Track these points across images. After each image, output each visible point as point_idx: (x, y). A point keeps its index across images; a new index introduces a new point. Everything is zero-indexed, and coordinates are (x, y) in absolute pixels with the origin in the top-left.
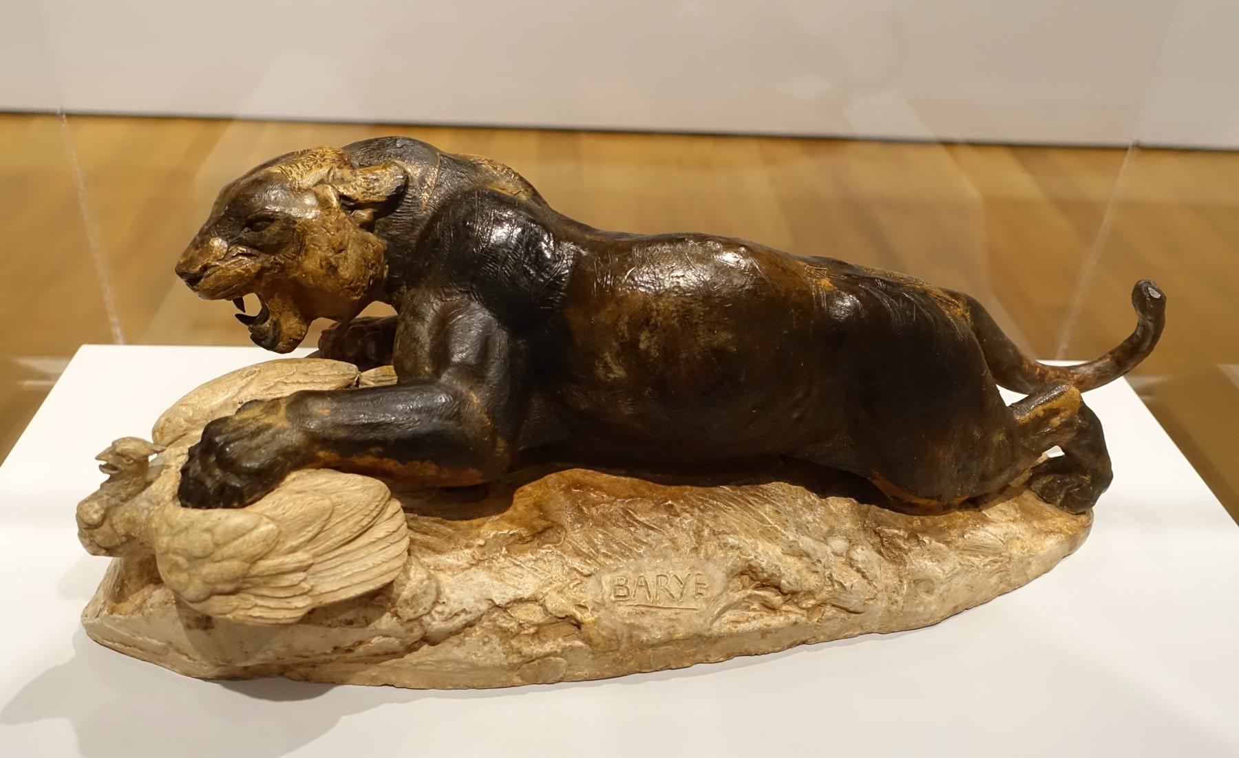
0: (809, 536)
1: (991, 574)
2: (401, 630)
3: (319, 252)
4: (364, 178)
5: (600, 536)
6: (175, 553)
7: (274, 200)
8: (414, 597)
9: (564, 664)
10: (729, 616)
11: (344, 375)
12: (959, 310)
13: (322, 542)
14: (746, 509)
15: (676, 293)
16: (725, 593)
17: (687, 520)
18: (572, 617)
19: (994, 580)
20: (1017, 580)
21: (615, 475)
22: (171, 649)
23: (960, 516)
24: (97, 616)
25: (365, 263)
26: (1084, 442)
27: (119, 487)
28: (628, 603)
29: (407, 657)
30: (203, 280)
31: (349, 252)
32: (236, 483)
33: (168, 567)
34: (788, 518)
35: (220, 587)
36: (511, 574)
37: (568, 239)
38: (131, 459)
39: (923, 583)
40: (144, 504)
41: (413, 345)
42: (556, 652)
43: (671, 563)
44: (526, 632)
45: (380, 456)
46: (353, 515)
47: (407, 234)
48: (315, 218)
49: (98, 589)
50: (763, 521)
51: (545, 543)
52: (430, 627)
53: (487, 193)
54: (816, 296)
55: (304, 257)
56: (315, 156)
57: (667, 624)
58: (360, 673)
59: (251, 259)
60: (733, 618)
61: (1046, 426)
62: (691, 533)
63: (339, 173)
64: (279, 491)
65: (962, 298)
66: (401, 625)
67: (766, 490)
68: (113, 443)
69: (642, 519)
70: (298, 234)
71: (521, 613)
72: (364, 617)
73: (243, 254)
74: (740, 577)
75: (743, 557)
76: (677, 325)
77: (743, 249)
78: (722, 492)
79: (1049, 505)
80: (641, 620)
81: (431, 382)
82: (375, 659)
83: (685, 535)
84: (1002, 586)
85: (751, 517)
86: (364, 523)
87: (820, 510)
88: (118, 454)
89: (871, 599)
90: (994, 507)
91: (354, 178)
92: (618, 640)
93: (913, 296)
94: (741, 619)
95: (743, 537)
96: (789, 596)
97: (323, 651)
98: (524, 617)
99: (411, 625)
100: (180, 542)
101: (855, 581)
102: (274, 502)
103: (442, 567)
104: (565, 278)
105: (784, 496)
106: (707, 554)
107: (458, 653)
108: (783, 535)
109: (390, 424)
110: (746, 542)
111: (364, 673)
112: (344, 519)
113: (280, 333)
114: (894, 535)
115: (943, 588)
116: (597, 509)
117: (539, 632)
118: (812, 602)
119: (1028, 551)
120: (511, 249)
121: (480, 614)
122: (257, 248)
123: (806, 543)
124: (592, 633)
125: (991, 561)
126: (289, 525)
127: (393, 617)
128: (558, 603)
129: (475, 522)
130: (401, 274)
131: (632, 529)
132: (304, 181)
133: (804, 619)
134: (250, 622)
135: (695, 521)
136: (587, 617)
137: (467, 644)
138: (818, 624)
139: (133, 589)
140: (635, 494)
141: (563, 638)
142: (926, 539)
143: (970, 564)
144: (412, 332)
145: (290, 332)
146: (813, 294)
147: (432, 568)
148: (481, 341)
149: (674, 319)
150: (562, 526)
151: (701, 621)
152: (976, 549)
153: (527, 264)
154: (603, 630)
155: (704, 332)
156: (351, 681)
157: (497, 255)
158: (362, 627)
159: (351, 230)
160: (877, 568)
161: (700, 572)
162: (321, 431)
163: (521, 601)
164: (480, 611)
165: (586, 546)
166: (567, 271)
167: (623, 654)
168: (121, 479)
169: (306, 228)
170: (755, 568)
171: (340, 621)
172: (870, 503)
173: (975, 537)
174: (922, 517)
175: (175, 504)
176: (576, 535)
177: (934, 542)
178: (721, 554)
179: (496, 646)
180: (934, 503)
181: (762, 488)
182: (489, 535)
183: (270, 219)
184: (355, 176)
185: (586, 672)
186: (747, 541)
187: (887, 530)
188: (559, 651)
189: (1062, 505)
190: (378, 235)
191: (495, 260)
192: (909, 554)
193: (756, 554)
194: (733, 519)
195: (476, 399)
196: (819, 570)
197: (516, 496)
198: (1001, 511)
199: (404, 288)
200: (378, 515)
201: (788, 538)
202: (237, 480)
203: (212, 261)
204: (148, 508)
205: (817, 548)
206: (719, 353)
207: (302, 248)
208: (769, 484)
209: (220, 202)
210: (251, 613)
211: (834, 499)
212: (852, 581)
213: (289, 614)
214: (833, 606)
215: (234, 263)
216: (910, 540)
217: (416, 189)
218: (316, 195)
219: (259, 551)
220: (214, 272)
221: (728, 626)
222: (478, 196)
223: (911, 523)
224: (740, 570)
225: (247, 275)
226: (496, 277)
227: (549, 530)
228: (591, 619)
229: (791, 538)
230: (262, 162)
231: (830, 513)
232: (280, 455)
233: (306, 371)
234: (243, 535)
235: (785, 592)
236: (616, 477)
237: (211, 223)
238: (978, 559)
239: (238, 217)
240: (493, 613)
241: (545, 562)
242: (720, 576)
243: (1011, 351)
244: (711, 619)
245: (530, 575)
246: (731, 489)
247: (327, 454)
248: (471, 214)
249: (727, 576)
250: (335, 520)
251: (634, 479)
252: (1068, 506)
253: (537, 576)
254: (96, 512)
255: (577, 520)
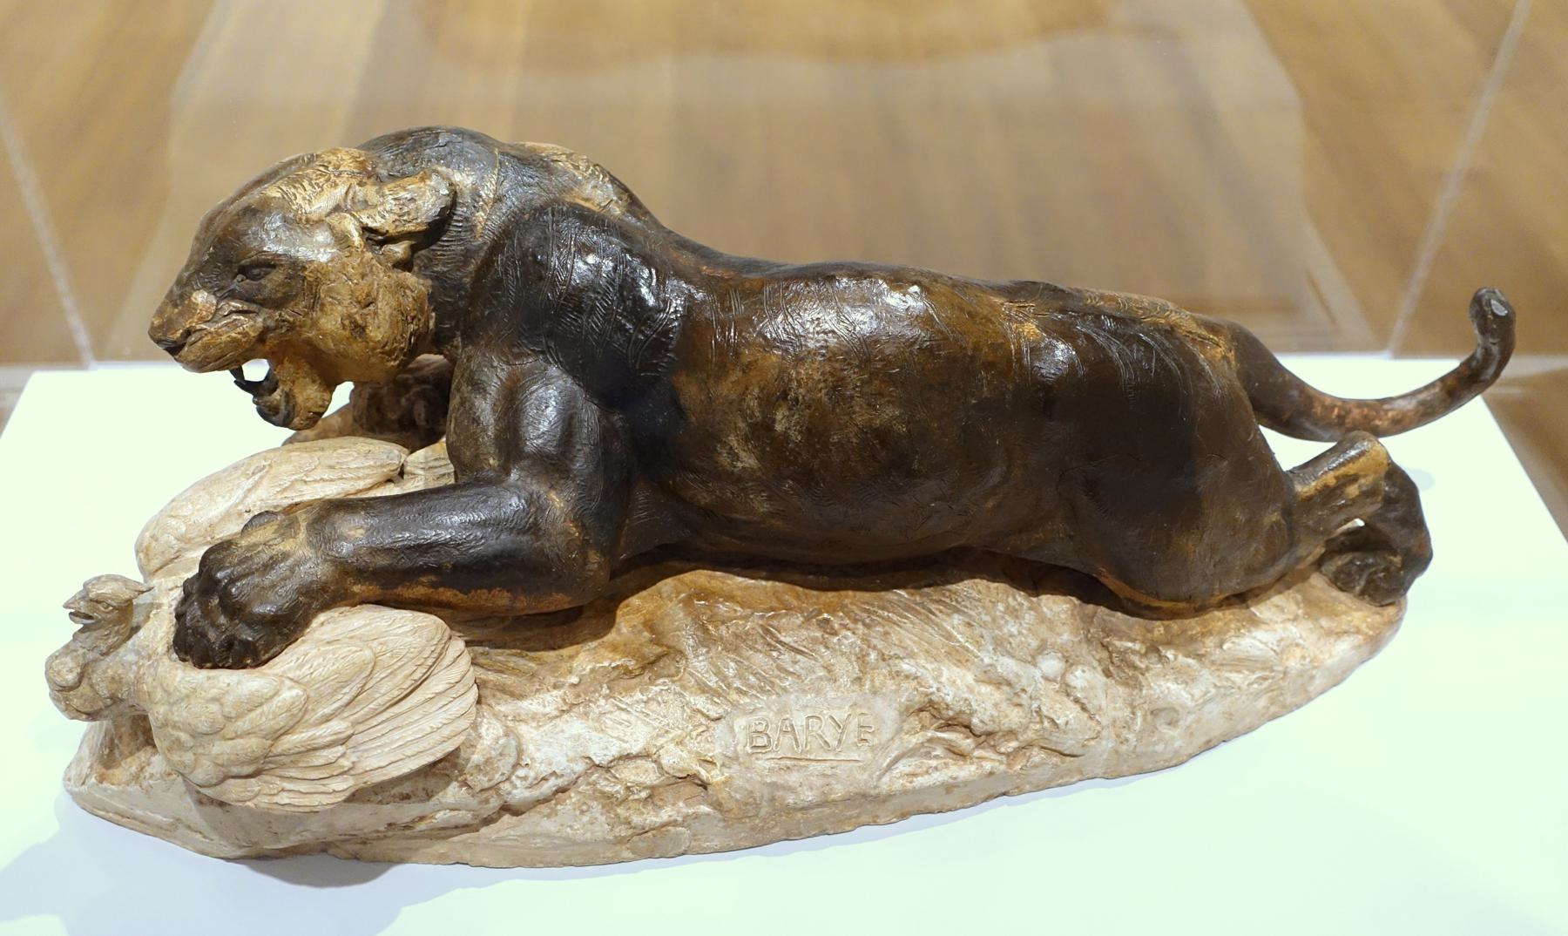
0: (1012, 656)
1: (1258, 695)
2: (473, 802)
3: (340, 308)
4: (395, 199)
5: (732, 664)
6: (175, 727)
7: (273, 241)
8: (488, 761)
9: (686, 835)
10: (903, 767)
11: (382, 466)
12: (1219, 350)
13: (361, 707)
14: (929, 621)
15: (823, 355)
16: (898, 736)
17: (849, 640)
18: (695, 776)
19: (1262, 703)
20: (1294, 700)
21: (753, 578)
22: (180, 825)
23: (1219, 617)
24: (83, 783)
25: (403, 316)
26: (1392, 515)
27: (97, 638)
28: (769, 756)
29: (484, 830)
30: (186, 348)
31: (379, 305)
32: (247, 635)
33: (166, 744)
34: (984, 632)
35: (235, 770)
36: (614, 721)
37: (679, 275)
38: (109, 605)
39: (1163, 713)
40: (131, 657)
41: (473, 428)
42: (676, 821)
43: (826, 700)
44: (636, 797)
45: (433, 585)
46: (403, 665)
47: (459, 270)
48: (332, 261)
49: (82, 743)
50: (949, 637)
51: (659, 676)
52: (510, 796)
53: (565, 209)
54: (1016, 350)
55: (319, 313)
56: (326, 167)
57: (819, 782)
58: (424, 850)
59: (250, 318)
60: (908, 770)
61: (1341, 496)
62: (853, 658)
63: (360, 192)
64: (304, 641)
65: (1225, 331)
66: (473, 796)
67: (955, 593)
68: (85, 585)
69: (787, 640)
70: (310, 284)
71: (629, 773)
72: (424, 789)
73: (239, 312)
74: (918, 715)
75: (922, 689)
76: (825, 399)
77: (915, 288)
78: (896, 598)
79: (1345, 594)
80: (787, 777)
81: (497, 479)
82: (443, 833)
83: (844, 660)
84: (1273, 709)
85: (933, 632)
86: (417, 675)
87: (1029, 617)
88: (92, 600)
89: (1093, 739)
90: (1268, 602)
91: (381, 200)
92: (755, 803)
93: (1153, 338)
94: (919, 771)
95: (922, 662)
96: (983, 738)
97: (375, 828)
98: (633, 778)
99: (485, 795)
100: (180, 714)
101: (1071, 716)
102: (298, 659)
103: (523, 717)
104: (674, 333)
105: (979, 600)
106: (873, 686)
107: (549, 825)
108: (976, 657)
109: (445, 544)
110: (926, 669)
111: (429, 850)
112: (392, 672)
113: (294, 407)
114: (1127, 650)
115: (1190, 719)
116: (727, 627)
117: (653, 796)
118: (1014, 744)
119: (1311, 661)
120: (598, 293)
121: (575, 777)
122: (256, 302)
123: (1007, 666)
124: (723, 796)
125: (1258, 678)
126: (319, 688)
127: (461, 787)
128: (675, 758)
129: (566, 652)
130: (453, 323)
131: (775, 654)
132: (313, 208)
133: (1002, 768)
134: (278, 811)
135: (859, 642)
136: (714, 776)
137: (559, 813)
138: (1023, 772)
139: (126, 753)
140: (777, 605)
141: (685, 801)
142: (1170, 654)
143: (1229, 684)
144: (471, 409)
145: (309, 404)
146: (1012, 346)
147: (510, 718)
148: (563, 421)
149: (820, 391)
150: (681, 652)
151: (865, 776)
152: (1239, 663)
153: (621, 315)
154: (736, 792)
155: (861, 408)
156: (414, 860)
157: (581, 303)
158: (423, 801)
159: (381, 275)
160: (1102, 695)
161: (864, 711)
162: (354, 560)
163: (628, 757)
164: (575, 773)
165: (715, 679)
166: (676, 324)
167: (764, 820)
168: (99, 628)
169: (319, 275)
170: (938, 703)
171: (394, 796)
172: (1098, 604)
173: (1238, 647)
174: (1166, 623)
175: (170, 659)
176: (699, 664)
177: (1181, 658)
178: (891, 685)
179: (598, 815)
180: (1182, 605)
181: (950, 591)
182: (584, 670)
183: (270, 264)
184: (383, 196)
185: (716, 843)
186: (928, 666)
187: (1118, 643)
188: (680, 819)
189: (1362, 593)
190: (418, 275)
191: (579, 309)
192: (1147, 674)
193: (939, 686)
194: (910, 636)
195: (558, 503)
196: (1023, 702)
197: (619, 613)
198: (1277, 606)
199: (458, 341)
200: (434, 663)
201: (982, 660)
202: (248, 632)
203: (197, 323)
204: (136, 663)
205: (1021, 672)
206: (882, 435)
207: (316, 302)
208: (960, 584)
209: (202, 237)
210: (276, 799)
211: (1048, 599)
212: (1067, 716)
213: (325, 800)
214: (1042, 748)
215: (226, 325)
216: (1149, 655)
217: (467, 207)
218: (331, 228)
219: (282, 724)
220: (201, 339)
221: (901, 781)
222: (553, 215)
223: (1151, 631)
224: (917, 707)
225: (244, 340)
226: (580, 333)
227: (665, 658)
228: (720, 778)
229: (987, 661)
230: (254, 176)
231: (1043, 620)
232: (302, 594)
233: (333, 462)
234: (261, 704)
235: (978, 733)
236: (753, 581)
237: (192, 269)
238: (1241, 676)
239: (228, 262)
240: (592, 774)
241: (659, 703)
242: (891, 715)
243: (1295, 393)
244: (878, 773)
245: (639, 722)
246: (908, 593)
247: (364, 588)
248: (544, 241)
249: (901, 714)
250: (379, 675)
251: (777, 583)
252: (1370, 595)
253: (648, 723)
254: (71, 671)
255: (702, 643)
